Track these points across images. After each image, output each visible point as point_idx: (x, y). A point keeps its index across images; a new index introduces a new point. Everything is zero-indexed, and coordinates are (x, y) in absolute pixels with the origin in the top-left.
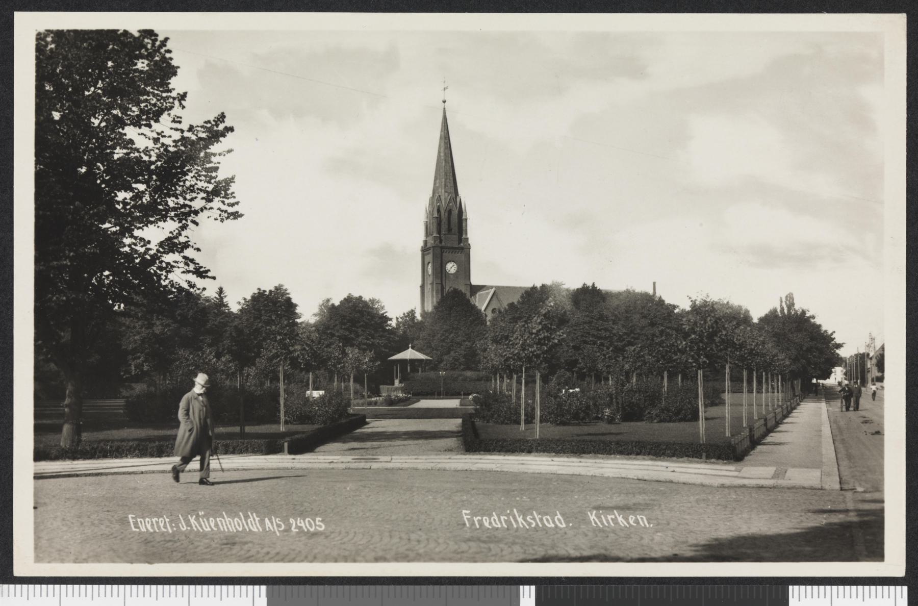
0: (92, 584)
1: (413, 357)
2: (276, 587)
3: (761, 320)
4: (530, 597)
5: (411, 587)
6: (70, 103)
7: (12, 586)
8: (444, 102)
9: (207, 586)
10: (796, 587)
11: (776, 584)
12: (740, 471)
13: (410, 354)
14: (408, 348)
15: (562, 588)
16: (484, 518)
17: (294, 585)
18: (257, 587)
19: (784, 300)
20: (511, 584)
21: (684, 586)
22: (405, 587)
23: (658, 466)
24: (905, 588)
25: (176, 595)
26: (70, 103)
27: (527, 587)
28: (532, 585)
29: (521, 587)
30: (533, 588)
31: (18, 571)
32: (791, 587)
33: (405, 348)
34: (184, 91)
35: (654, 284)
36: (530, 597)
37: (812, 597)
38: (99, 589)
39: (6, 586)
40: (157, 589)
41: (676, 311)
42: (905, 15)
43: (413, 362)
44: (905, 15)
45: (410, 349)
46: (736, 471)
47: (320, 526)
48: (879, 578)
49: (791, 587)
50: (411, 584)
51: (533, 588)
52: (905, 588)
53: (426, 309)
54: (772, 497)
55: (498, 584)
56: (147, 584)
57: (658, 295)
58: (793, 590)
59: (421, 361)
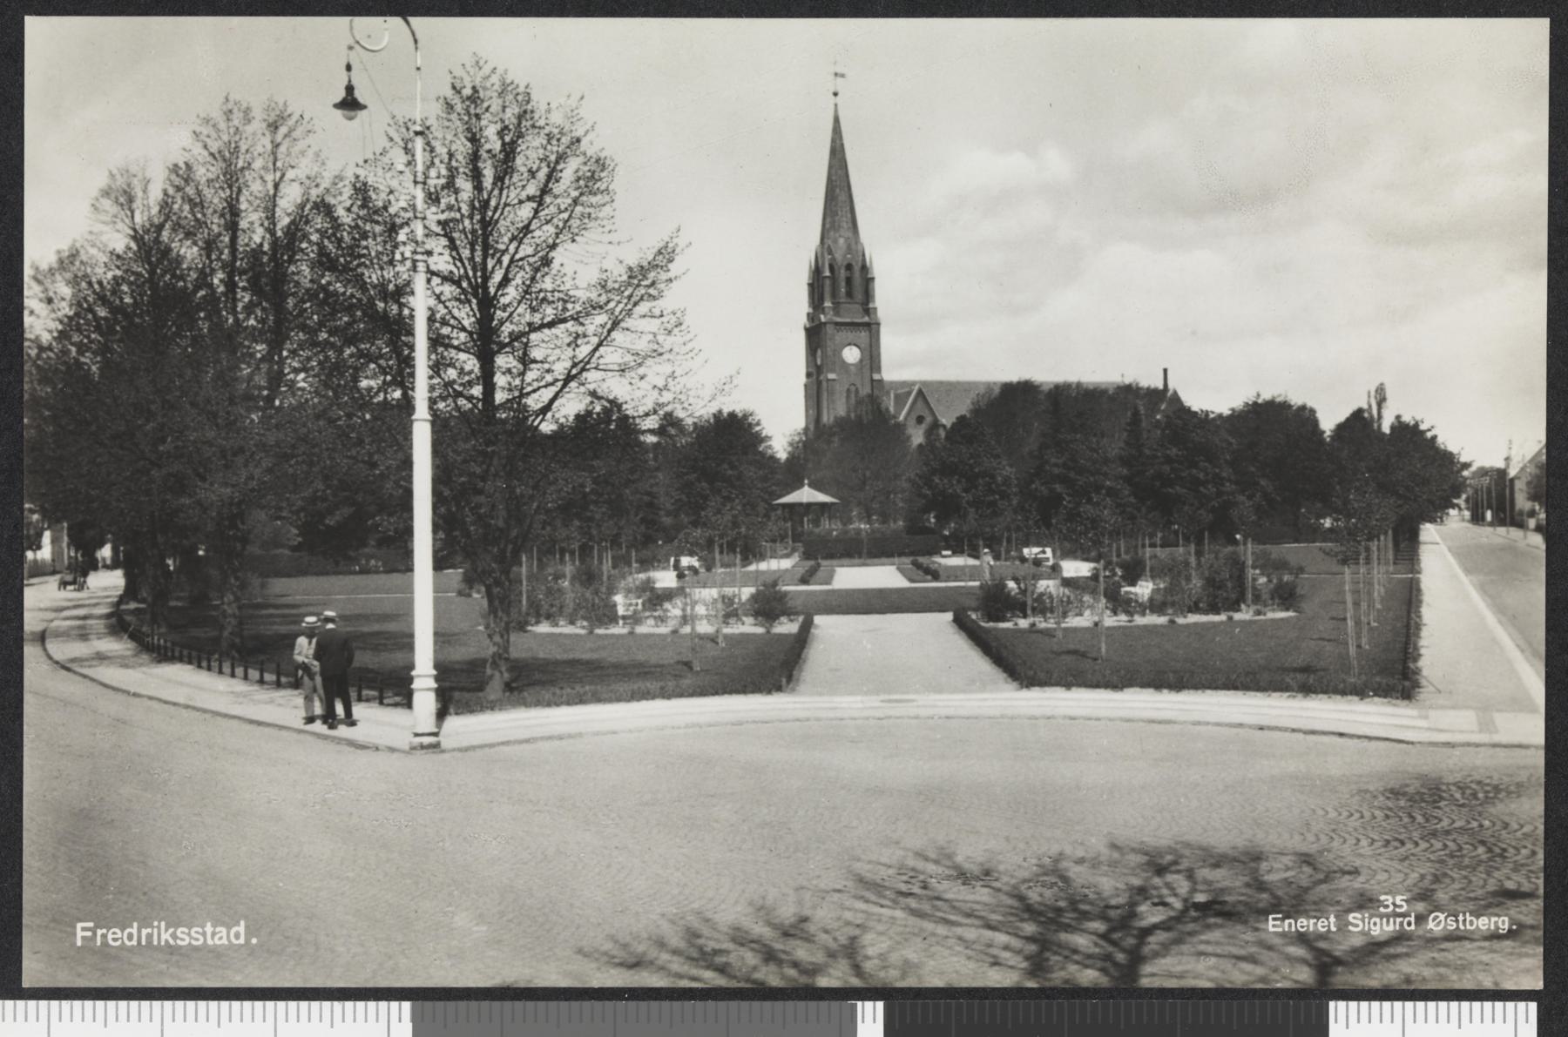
0: (277, 999)
1: (812, 500)
2: (428, 1004)
3: (1341, 428)
5: (440, 1004)
7: (20, 1003)
8: (835, 94)
10: (1342, 1004)
11: (1048, 997)
12: (1426, 717)
13: (806, 494)
14: (802, 485)
16: (242, 941)
18: (394, 1005)
19: (1373, 393)
20: (493, 999)
21: (1032, 1002)
22: (553, 1004)
23: (1308, 709)
24: (1533, 1006)
27: (869, 1005)
28: (1532, 1000)
29: (859, 1004)
30: (880, 1005)
31: (27, 983)
32: (1332, 1004)
33: (798, 485)
35: (1165, 371)
39: (9, 1003)
41: (1212, 416)
42: (27, 18)
43: (808, 507)
44: (27, 18)
45: (806, 488)
46: (1421, 717)
47: (197, 940)
48: (370, 990)
49: (1332, 1004)
50: (440, 999)
51: (880, 1005)
52: (1533, 1006)
56: (1398, 1000)
57: (1171, 386)
59: (823, 505)
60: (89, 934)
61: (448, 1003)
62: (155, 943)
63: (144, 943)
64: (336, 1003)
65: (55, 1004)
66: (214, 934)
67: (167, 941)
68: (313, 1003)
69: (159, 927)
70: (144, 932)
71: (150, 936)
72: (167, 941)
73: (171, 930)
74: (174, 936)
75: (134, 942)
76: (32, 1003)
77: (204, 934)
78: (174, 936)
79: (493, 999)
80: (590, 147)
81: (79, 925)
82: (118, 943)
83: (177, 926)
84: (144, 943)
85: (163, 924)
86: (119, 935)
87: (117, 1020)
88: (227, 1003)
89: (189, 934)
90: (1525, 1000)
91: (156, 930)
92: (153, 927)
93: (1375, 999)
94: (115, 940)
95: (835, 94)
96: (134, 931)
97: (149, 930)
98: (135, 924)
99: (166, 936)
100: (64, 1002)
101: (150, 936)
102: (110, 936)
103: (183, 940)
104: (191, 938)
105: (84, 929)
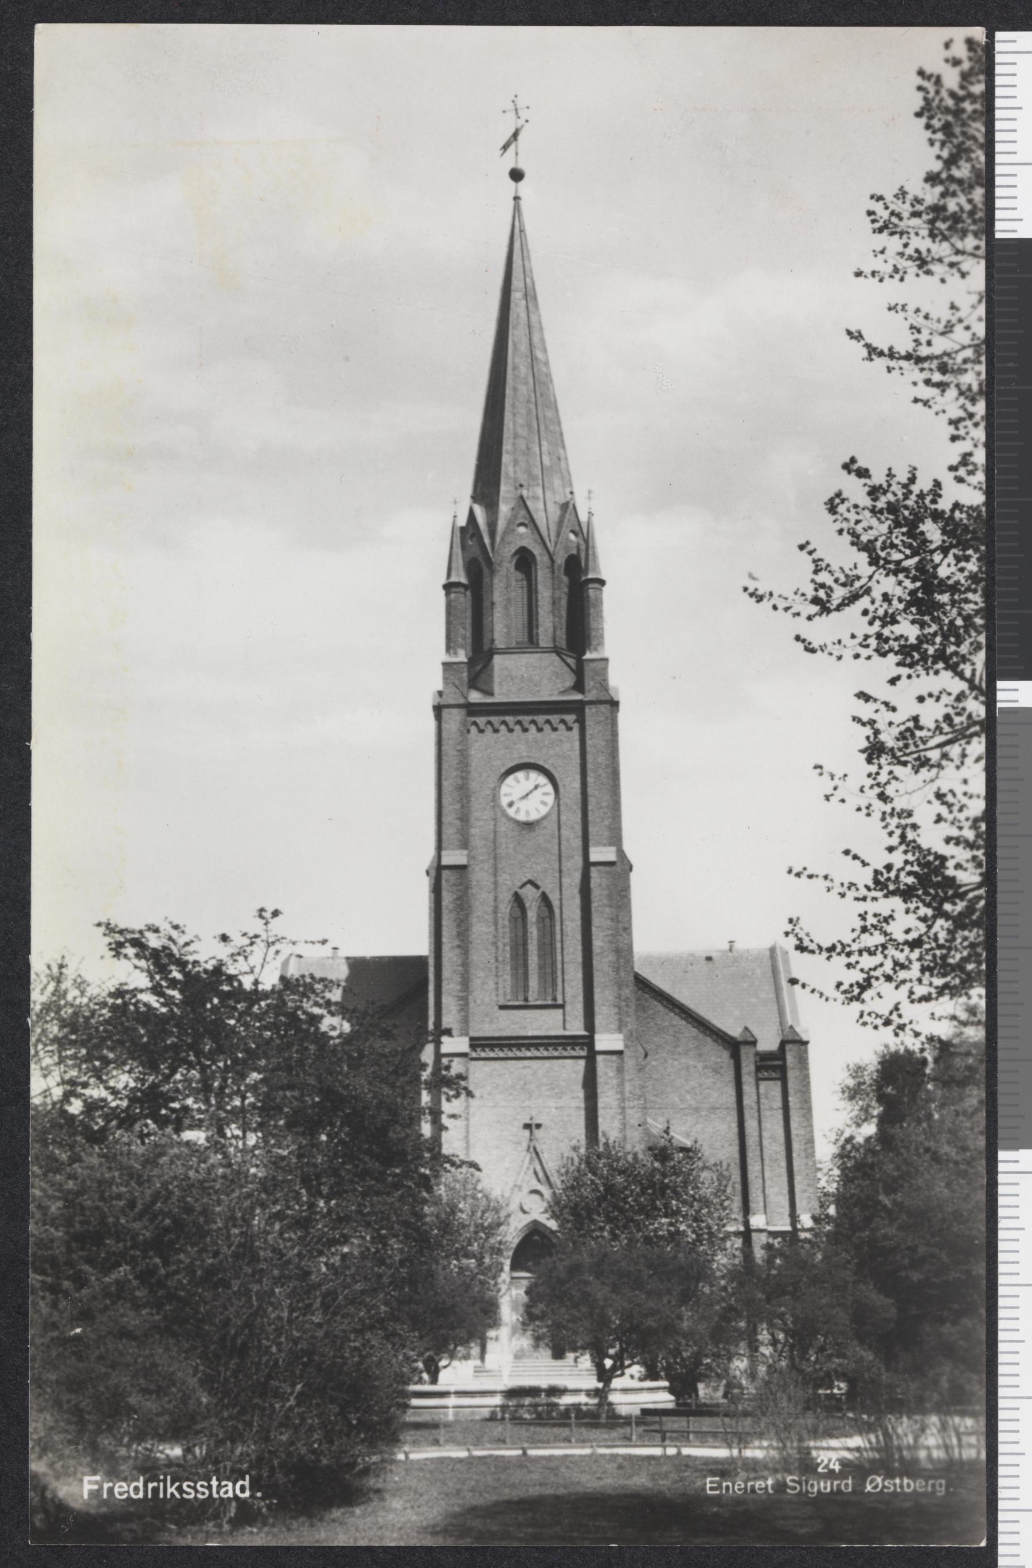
2: (1001, 1133)
4: (1017, 690)
6: (96, 1128)
7: (1001, 1550)
9: (1000, 1468)
10: (998, 226)
11: (988, 1184)
15: (1001, 533)
17: (995, 833)
18: (1001, 1167)
20: (996, 1071)
21: (997, 533)
24: (999, 35)
25: (1014, 1296)
26: (96, 1128)
27: (1000, 696)
29: (999, 705)
30: (1000, 684)
32: (998, 235)
34: (899, 187)
36: (1017, 690)
37: (1018, 1375)
38: (1005, 1443)
40: (1001, 119)
49: (998, 235)
50: (996, 1122)
53: (591, 586)
54: (49, 1280)
55: (995, 781)
58: (1003, 230)
60: (96, 1487)
61: (999, 1113)
62: (161, 1496)
63: (150, 1496)
64: (1000, 1225)
65: (1001, 1505)
66: (219, 1487)
67: (172, 1494)
68: (1000, 1248)
69: (165, 1481)
70: (150, 1486)
71: (156, 1490)
72: (172, 1494)
73: (177, 1484)
74: (180, 1489)
75: (141, 1495)
76: (1001, 1539)
77: (210, 1487)
78: (180, 1489)
79: (995, 1070)
80: (307, 974)
81: (86, 1479)
82: (125, 1496)
83: (181, 1480)
84: (150, 1496)
85: (169, 1478)
86: (126, 1489)
87: (1017, 1443)
88: (1000, 1356)
89: (195, 1488)
90: (996, 1375)
91: (161, 1484)
92: (159, 1481)
93: (993, 192)
94: (121, 1494)
95: (516, 175)
96: (141, 1484)
97: (155, 1484)
98: (141, 1479)
99: (171, 1490)
100: (1000, 1496)
101: (156, 1490)
102: (116, 1490)
103: (188, 1494)
104: (197, 1491)
105: (90, 1482)
